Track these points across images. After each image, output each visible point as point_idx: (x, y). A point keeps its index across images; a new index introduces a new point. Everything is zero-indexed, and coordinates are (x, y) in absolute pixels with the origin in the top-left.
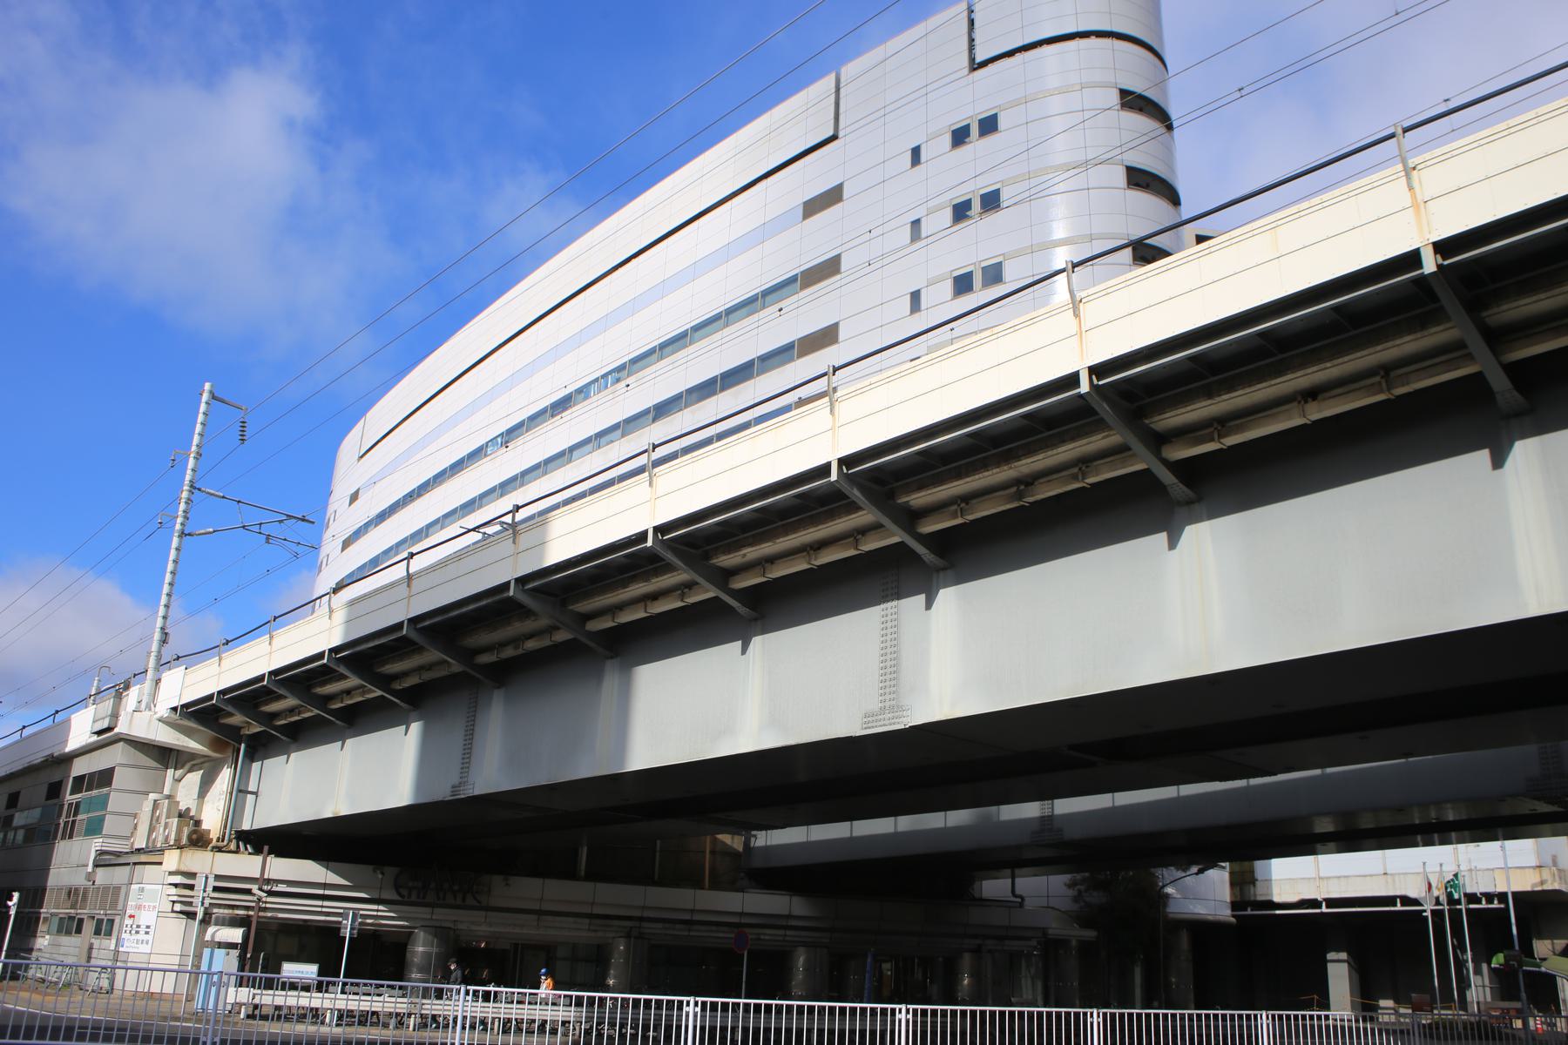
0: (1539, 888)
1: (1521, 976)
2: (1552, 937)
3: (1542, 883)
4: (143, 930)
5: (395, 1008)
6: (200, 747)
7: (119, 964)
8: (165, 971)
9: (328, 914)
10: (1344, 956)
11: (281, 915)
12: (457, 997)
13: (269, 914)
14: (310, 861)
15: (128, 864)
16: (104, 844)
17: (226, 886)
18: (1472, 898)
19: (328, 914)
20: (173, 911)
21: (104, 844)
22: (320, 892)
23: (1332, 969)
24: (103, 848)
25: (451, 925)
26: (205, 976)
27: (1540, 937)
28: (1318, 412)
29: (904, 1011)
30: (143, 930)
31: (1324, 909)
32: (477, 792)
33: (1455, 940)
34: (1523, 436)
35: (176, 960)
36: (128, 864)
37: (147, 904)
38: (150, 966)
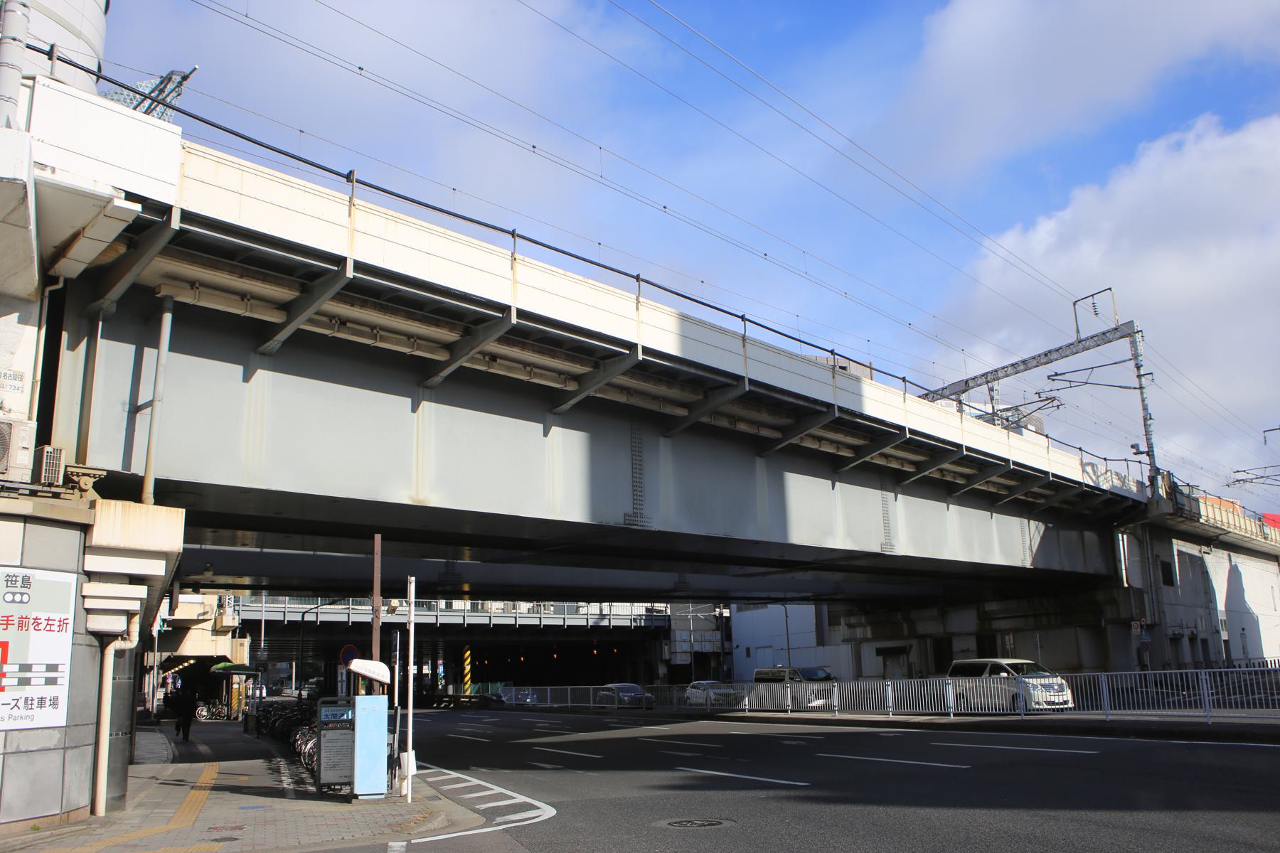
4: (38, 675)
34: (261, 369)
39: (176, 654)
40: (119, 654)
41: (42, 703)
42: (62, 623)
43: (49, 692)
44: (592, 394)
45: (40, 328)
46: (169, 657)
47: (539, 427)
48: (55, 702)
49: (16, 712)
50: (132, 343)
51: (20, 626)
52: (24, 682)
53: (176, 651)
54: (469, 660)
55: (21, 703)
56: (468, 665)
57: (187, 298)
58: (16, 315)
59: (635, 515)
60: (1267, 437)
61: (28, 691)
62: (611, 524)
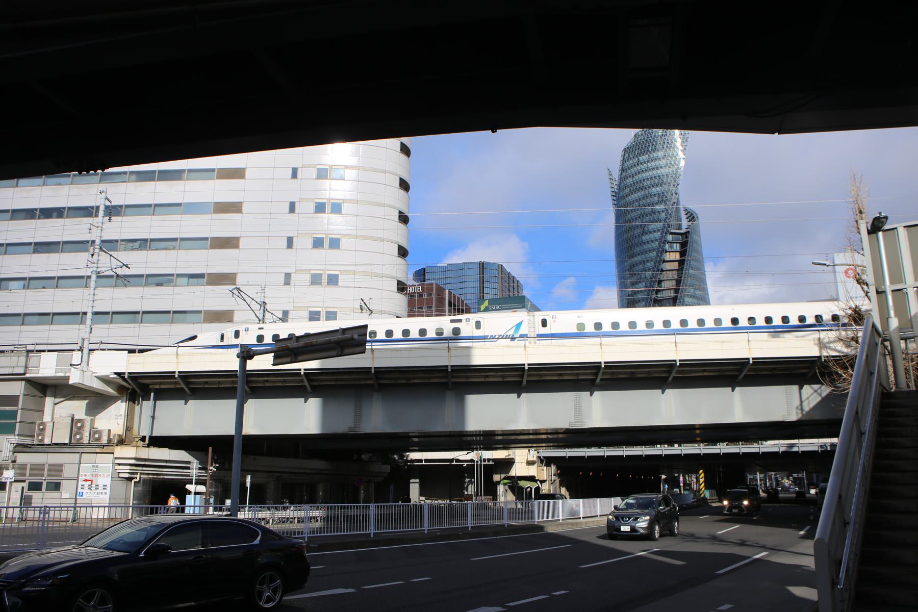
0: (508, 457)
1: (516, 487)
2: (500, 473)
3: (509, 455)
4: (101, 487)
5: (286, 515)
6: (115, 392)
7: (78, 505)
8: (87, 507)
9: (182, 475)
10: (417, 480)
11: (166, 477)
12: (160, 511)
13: (162, 477)
14: (183, 451)
15: (79, 453)
16: (19, 440)
17: (141, 463)
18: (485, 460)
19: (182, 475)
20: (119, 477)
21: (19, 440)
22: (143, 463)
23: (391, 487)
24: (19, 442)
25: (222, 478)
26: (131, 508)
27: (496, 474)
28: (706, 374)
29: (162, 509)
30: (101, 487)
31: (424, 463)
32: (368, 431)
33: (739, 487)
34: (738, 387)
35: (123, 501)
36: (79, 453)
37: (102, 474)
38: (93, 505)
39: (508, 475)
40: (135, 482)
41: (102, 493)
42: (108, 476)
43: (104, 491)
44: (746, 373)
45: (126, 402)
46: (505, 477)
47: (730, 389)
48: (106, 493)
49: (94, 495)
50: (516, 393)
51: (95, 476)
52: (96, 489)
53: (508, 474)
54: (703, 475)
55: (96, 493)
56: (702, 478)
57: (157, 387)
58: (120, 401)
59: (355, 427)
60: (137, 315)
61: (98, 491)
62: (341, 432)
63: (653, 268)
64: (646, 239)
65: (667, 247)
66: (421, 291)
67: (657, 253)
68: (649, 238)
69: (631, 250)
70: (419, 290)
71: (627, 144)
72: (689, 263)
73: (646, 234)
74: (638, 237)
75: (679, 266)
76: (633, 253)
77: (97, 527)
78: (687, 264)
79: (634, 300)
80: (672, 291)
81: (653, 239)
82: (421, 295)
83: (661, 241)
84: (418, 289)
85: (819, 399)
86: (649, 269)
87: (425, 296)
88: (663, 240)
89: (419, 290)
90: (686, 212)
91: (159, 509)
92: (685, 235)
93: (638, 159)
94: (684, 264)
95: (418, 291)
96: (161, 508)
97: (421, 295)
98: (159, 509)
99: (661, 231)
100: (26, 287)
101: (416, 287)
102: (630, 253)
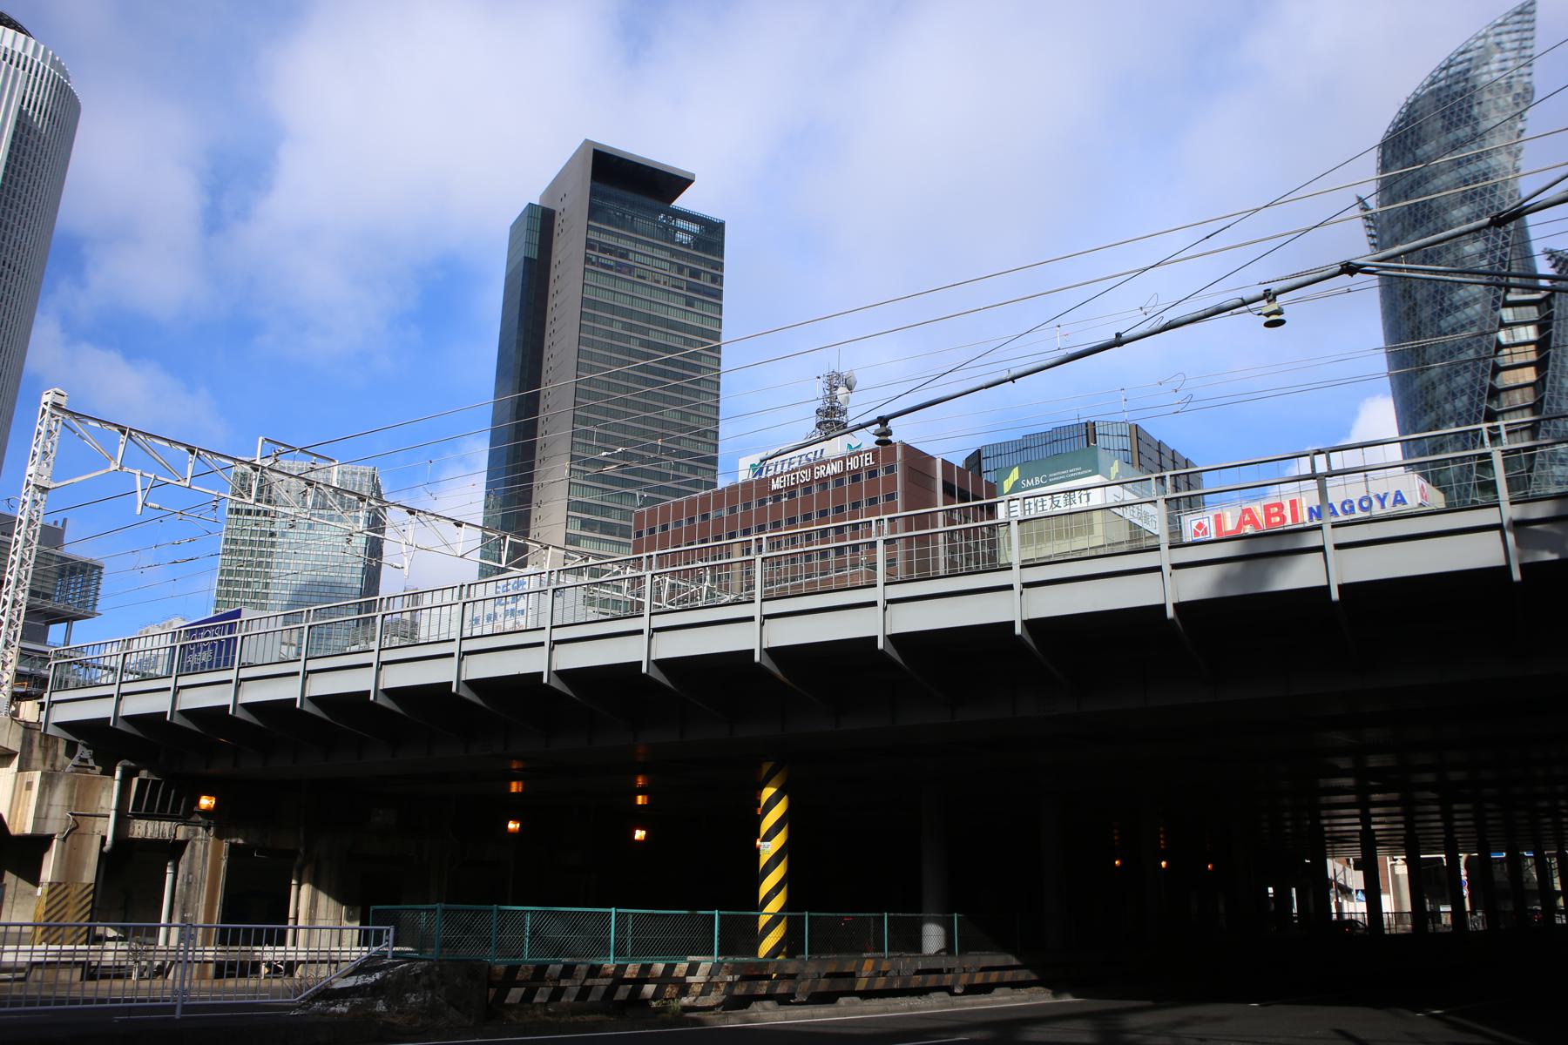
63: (1472, 387)
64: (1449, 326)
65: (1503, 336)
66: (872, 463)
67: (1474, 375)
68: (1454, 320)
69: (1415, 315)
70: (868, 461)
71: (1385, 130)
72: (1559, 363)
73: (1448, 313)
74: (1419, 287)
75: (1538, 374)
76: (1420, 322)
77: (70, 981)
78: (1556, 366)
79: (1437, 168)
80: (1529, 391)
81: (1464, 322)
82: (873, 473)
83: (1473, 392)
84: (866, 459)
85: (1384, 911)
86: (1462, 391)
87: (882, 474)
88: (1478, 387)
89: (868, 461)
90: (1553, 261)
91: (385, 932)
92: (1545, 304)
93: (1414, 155)
94: (1548, 347)
95: (866, 464)
96: (388, 931)
97: (873, 473)
98: (385, 932)
99: (1475, 345)
100: (38, 560)
101: (861, 456)
102: (1412, 139)
